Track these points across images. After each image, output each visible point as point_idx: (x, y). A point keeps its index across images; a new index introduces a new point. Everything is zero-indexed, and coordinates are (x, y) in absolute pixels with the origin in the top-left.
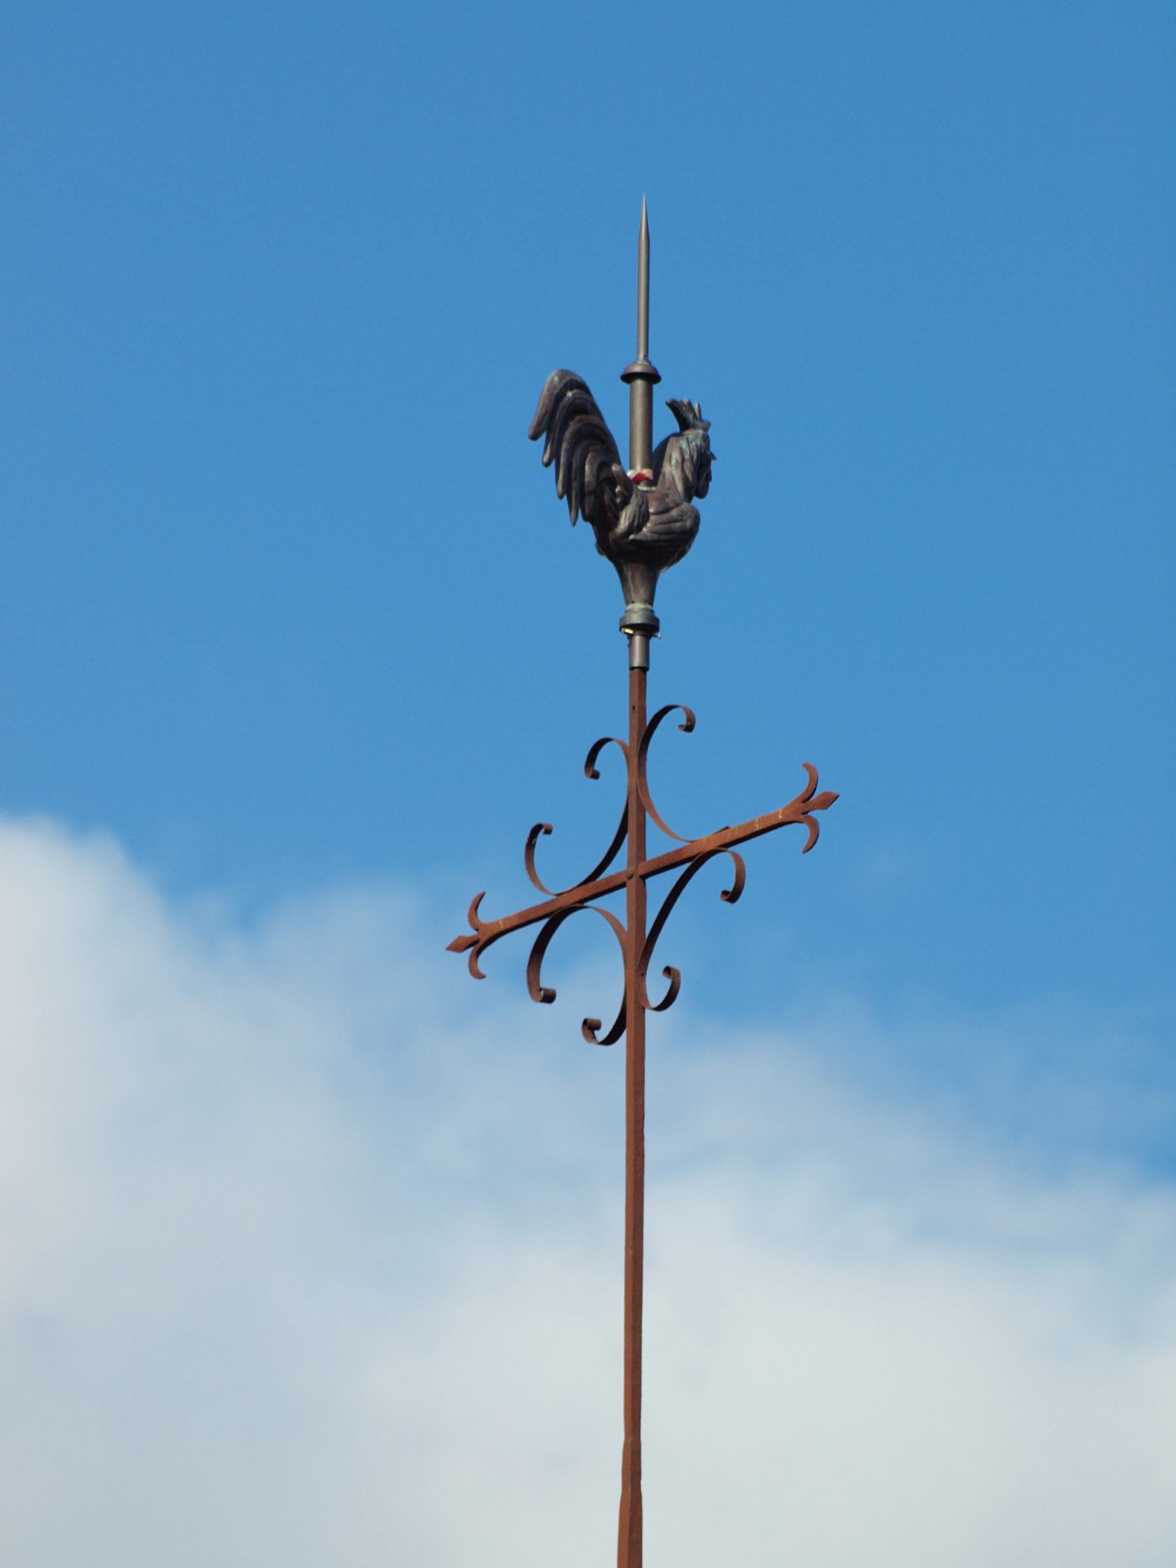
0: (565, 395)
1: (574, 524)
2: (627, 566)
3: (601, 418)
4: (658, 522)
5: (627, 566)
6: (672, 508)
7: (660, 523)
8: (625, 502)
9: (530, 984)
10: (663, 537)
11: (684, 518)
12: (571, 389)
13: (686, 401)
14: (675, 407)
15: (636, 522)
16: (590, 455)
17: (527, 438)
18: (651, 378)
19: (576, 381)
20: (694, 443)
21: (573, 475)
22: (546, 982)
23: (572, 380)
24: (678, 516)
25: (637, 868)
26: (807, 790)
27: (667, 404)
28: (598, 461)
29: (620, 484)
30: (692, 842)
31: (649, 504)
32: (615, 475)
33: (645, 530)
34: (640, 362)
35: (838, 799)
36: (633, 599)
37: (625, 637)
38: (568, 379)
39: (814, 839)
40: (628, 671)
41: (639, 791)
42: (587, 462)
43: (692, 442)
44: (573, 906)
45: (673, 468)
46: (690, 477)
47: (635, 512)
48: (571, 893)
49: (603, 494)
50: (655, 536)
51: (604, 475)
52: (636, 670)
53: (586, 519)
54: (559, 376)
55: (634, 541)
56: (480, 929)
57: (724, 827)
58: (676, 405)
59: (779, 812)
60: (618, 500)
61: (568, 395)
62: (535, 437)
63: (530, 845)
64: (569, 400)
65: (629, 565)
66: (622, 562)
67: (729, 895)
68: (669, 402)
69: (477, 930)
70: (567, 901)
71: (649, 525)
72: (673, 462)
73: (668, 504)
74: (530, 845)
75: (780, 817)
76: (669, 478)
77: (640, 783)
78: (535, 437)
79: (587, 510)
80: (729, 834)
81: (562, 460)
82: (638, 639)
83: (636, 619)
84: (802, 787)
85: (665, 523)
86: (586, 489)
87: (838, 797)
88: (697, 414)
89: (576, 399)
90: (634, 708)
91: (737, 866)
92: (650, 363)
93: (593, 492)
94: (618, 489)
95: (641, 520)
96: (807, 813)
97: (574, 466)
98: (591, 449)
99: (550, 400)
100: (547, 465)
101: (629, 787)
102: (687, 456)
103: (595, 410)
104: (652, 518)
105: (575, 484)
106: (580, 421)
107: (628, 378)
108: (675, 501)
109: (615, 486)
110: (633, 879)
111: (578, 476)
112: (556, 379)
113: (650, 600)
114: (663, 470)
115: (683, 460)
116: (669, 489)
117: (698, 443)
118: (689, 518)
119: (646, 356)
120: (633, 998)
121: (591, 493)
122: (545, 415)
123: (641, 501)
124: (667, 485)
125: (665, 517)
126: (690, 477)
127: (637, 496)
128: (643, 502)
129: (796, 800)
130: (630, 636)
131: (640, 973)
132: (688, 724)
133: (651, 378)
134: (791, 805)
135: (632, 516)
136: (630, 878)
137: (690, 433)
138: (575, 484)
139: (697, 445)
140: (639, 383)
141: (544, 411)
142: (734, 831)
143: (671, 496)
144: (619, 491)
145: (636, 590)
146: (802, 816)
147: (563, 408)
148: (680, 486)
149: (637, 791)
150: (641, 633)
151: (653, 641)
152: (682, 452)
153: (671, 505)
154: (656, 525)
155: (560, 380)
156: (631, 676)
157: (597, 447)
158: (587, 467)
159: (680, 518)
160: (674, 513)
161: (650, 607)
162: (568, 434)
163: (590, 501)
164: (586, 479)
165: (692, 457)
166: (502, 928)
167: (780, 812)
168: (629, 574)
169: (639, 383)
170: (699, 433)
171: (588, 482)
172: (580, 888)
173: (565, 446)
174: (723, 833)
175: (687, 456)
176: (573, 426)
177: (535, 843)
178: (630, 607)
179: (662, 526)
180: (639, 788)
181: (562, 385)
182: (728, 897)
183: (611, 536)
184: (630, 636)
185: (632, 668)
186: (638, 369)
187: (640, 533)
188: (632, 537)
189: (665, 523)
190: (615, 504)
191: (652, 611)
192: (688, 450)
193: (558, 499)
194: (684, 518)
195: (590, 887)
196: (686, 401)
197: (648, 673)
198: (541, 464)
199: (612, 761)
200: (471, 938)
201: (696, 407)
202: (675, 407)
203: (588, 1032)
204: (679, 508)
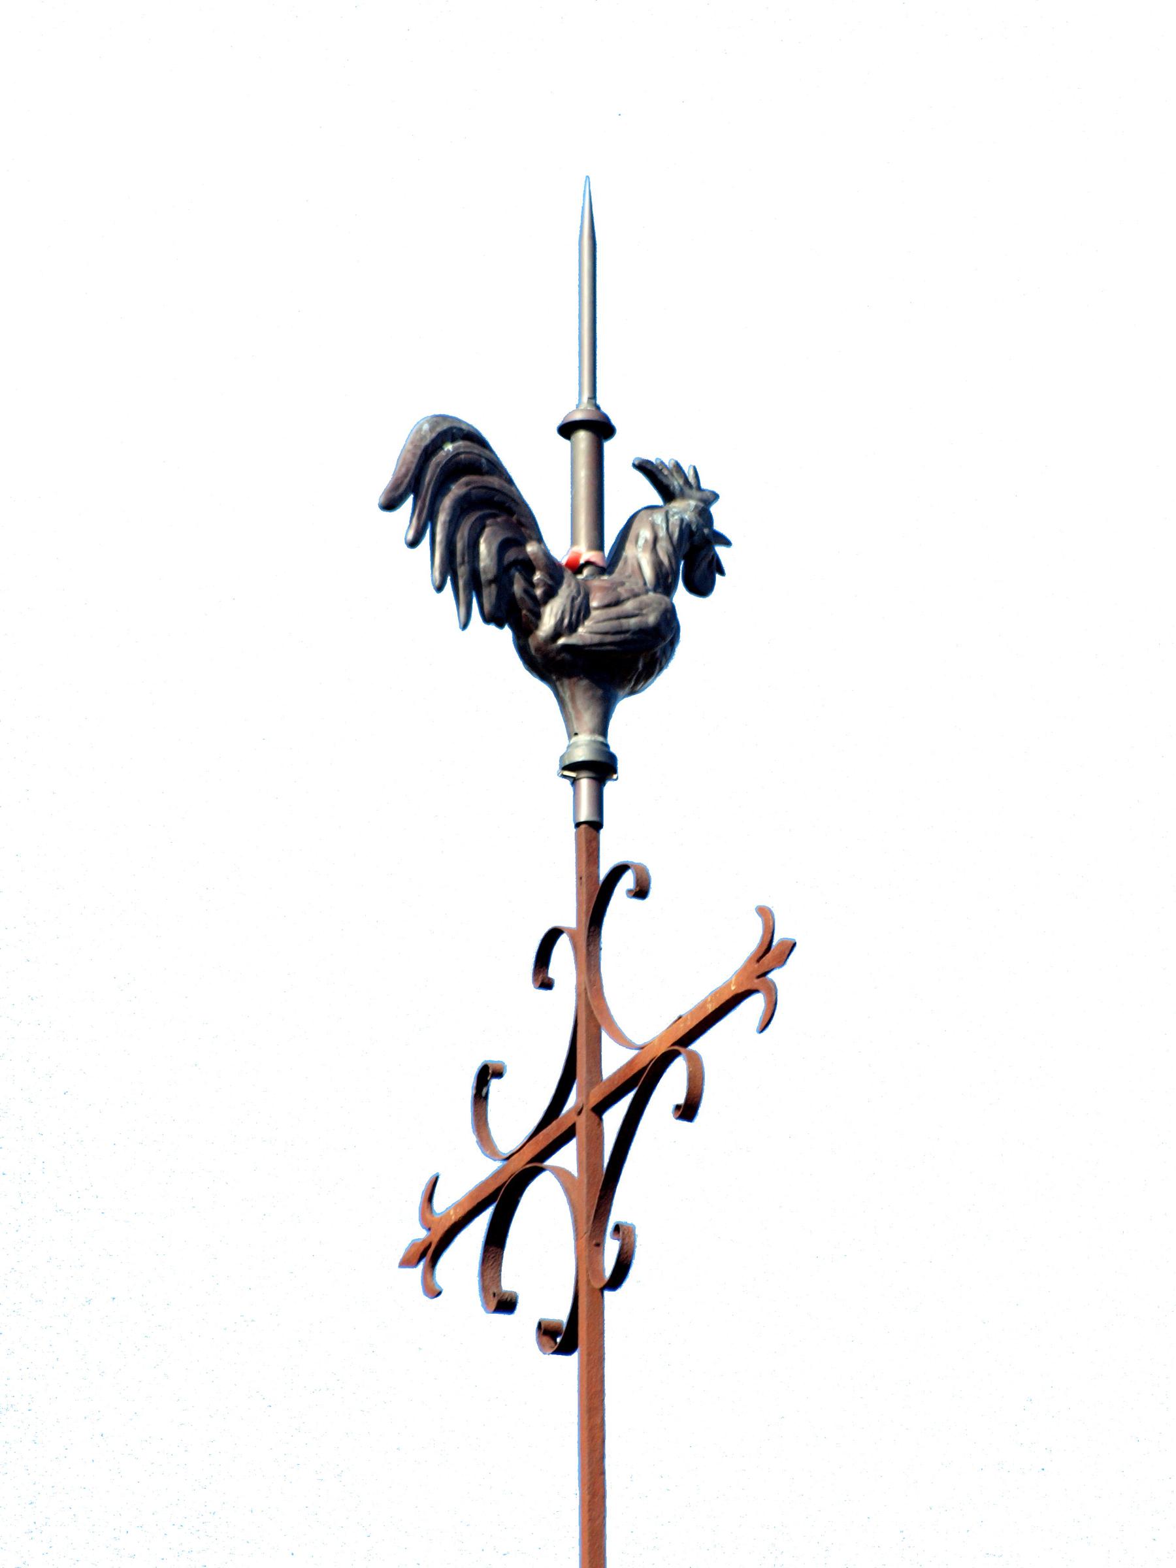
0: (441, 448)
1: (465, 626)
2: (562, 685)
3: (510, 481)
4: (601, 618)
5: (562, 685)
6: (628, 599)
7: (604, 620)
8: (550, 593)
9: (484, 1289)
10: (609, 638)
11: (644, 612)
12: (453, 440)
14: (646, 468)
15: (566, 621)
16: (487, 531)
18: (601, 429)
19: (461, 430)
20: (676, 517)
21: (459, 559)
22: (508, 1283)
24: (634, 609)
25: (588, 1097)
28: (500, 539)
29: (539, 570)
31: (591, 597)
32: (532, 558)
33: (581, 630)
35: (796, 950)
36: (577, 731)
37: (568, 782)
39: (772, 1008)
41: (589, 994)
42: (482, 541)
44: (524, 1168)
45: (640, 550)
47: (565, 606)
48: (522, 1151)
49: (511, 583)
50: (597, 639)
51: (511, 555)
53: (488, 619)
54: (430, 424)
55: (565, 647)
56: (432, 1226)
57: (676, 1018)
58: (649, 467)
59: (731, 982)
60: (539, 592)
61: (446, 449)
62: (390, 504)
63: (480, 1097)
64: (447, 454)
65: (566, 682)
66: (554, 677)
68: (636, 463)
70: (519, 1164)
71: (587, 623)
72: (641, 542)
73: (620, 594)
74: (480, 1097)
75: (733, 988)
76: (633, 565)
77: (590, 981)
78: (390, 504)
79: (487, 607)
80: (682, 1025)
82: (585, 784)
83: (581, 755)
84: (752, 941)
85: (610, 619)
86: (483, 578)
87: (794, 945)
88: (691, 479)
89: (458, 454)
90: (581, 878)
93: (494, 580)
94: (537, 576)
95: (574, 616)
96: (765, 974)
97: (460, 546)
98: (488, 522)
99: (414, 455)
100: (413, 544)
102: (662, 533)
103: (496, 467)
104: (594, 613)
105: (462, 571)
106: (467, 484)
108: (632, 590)
109: (533, 573)
111: (466, 558)
112: (426, 427)
113: (603, 729)
115: (656, 539)
116: (630, 576)
117: (686, 517)
118: (654, 610)
120: (585, 1279)
121: (490, 582)
122: (405, 475)
123: (575, 591)
124: (629, 571)
125: (614, 611)
127: (569, 586)
128: (579, 593)
129: (750, 960)
130: (574, 781)
131: (594, 1242)
132: (638, 889)
133: (601, 429)
135: (560, 612)
139: (682, 520)
140: (582, 436)
141: (403, 470)
142: (686, 1019)
143: (627, 584)
144: (538, 579)
145: (578, 719)
146: (756, 981)
147: (438, 464)
148: (648, 573)
149: (586, 993)
150: (591, 774)
151: (609, 788)
152: (654, 527)
153: (625, 595)
154: (598, 622)
155: (432, 429)
157: (499, 520)
158: (483, 548)
159: (637, 612)
160: (629, 606)
161: (601, 739)
162: (447, 503)
163: (490, 593)
164: (482, 564)
165: (670, 535)
166: (454, 1218)
167: (733, 982)
168: (567, 696)
169: (583, 437)
170: (689, 505)
171: (485, 567)
174: (675, 1025)
175: (662, 533)
176: (456, 490)
178: (574, 739)
180: (588, 990)
181: (434, 435)
182: (680, 1113)
183: (532, 642)
186: (579, 416)
187: (574, 635)
188: (562, 641)
189: (610, 619)
190: (533, 597)
191: (607, 746)
192: (664, 525)
194: (644, 612)
195: (541, 1137)
197: (602, 831)
199: (563, 956)
200: (424, 1241)
201: (686, 468)
202: (646, 468)
203: (545, 1339)
204: (638, 600)
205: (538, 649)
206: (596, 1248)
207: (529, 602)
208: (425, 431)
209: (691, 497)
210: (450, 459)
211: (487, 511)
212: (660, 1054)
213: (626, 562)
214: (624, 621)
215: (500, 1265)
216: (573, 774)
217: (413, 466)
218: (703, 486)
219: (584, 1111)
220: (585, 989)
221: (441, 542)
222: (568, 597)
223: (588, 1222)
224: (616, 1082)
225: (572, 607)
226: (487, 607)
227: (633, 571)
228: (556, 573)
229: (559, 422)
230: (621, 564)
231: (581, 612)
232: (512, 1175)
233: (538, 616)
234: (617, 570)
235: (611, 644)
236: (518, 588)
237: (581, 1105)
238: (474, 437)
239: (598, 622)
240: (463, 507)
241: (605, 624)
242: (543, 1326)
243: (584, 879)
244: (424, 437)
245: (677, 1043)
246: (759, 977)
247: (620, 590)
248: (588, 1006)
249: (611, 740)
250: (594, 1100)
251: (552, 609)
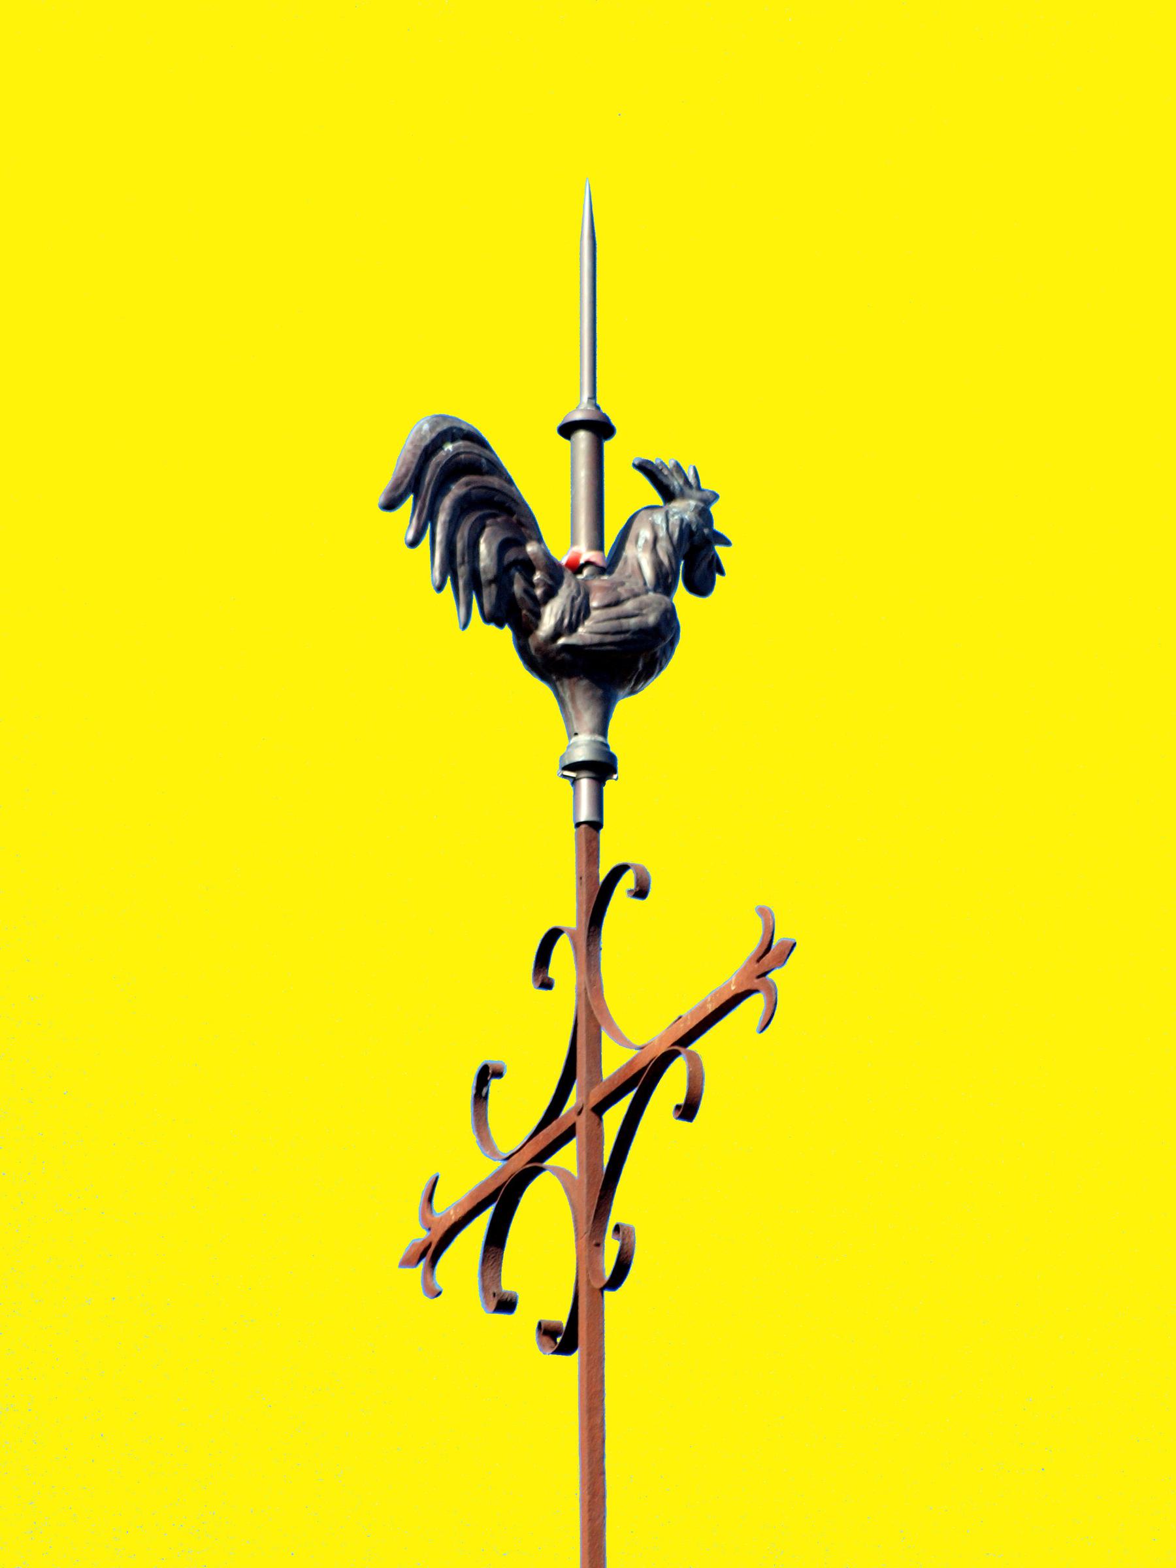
0: (441, 448)
1: (465, 626)
2: (562, 685)
3: (510, 481)
4: (601, 618)
5: (562, 685)
6: (628, 599)
7: (604, 620)
8: (550, 593)
9: (484, 1289)
10: (609, 638)
11: (644, 612)
12: (453, 440)
14: (646, 469)
15: (566, 621)
16: (487, 531)
17: (377, 506)
18: (601, 429)
19: (461, 430)
20: (676, 517)
21: (459, 559)
22: (508, 1283)
23: (451, 429)
24: (634, 609)
26: (760, 946)
28: (500, 539)
29: (539, 570)
30: (642, 1048)
31: (591, 597)
32: (532, 558)
33: (581, 630)
36: (577, 731)
37: (568, 782)
39: (772, 1008)
40: (574, 830)
42: (482, 541)
43: (673, 516)
44: (524, 1168)
45: (640, 550)
46: (666, 561)
47: (565, 606)
48: (522, 1151)
49: (511, 583)
50: (597, 639)
51: (511, 555)
53: (488, 619)
54: (430, 424)
55: (565, 647)
57: (676, 1018)
58: (649, 467)
59: (731, 982)
60: (539, 592)
61: (446, 449)
62: (391, 504)
63: (480, 1097)
64: (447, 454)
65: (566, 682)
66: (554, 677)
68: (636, 463)
70: (519, 1164)
71: (587, 623)
72: (641, 542)
73: (620, 594)
74: (480, 1097)
76: (633, 565)
77: (590, 981)
78: (391, 504)
79: (487, 607)
80: (682, 1025)
81: (439, 537)
82: (585, 784)
84: (752, 941)
85: (610, 619)
86: (483, 578)
87: (795, 944)
88: (691, 479)
89: (458, 454)
90: (581, 878)
91: (689, 1067)
93: (494, 580)
94: (537, 576)
95: (574, 616)
97: (460, 546)
98: (488, 522)
99: (414, 455)
100: (414, 544)
102: (662, 533)
103: (495, 467)
104: (594, 613)
105: (462, 571)
106: (467, 484)
107: (567, 430)
108: (632, 590)
109: (533, 573)
110: (582, 1114)
111: (466, 558)
112: (426, 427)
113: (603, 729)
115: (656, 539)
116: (630, 576)
117: (686, 517)
118: (654, 610)
119: (593, 396)
121: (490, 582)
122: (405, 475)
123: (575, 591)
124: (629, 571)
125: (614, 611)
127: (569, 586)
128: (579, 593)
130: (574, 781)
131: (594, 1242)
132: (638, 889)
133: (601, 429)
135: (560, 612)
136: (580, 1113)
138: (462, 571)
139: (682, 520)
140: (582, 436)
141: (403, 470)
142: (686, 1020)
143: (627, 584)
144: (538, 579)
145: (578, 719)
146: (756, 981)
147: (438, 464)
148: (648, 573)
149: (586, 993)
150: (591, 774)
152: (654, 527)
153: (625, 595)
154: (598, 622)
155: (432, 429)
156: (577, 836)
157: (499, 520)
158: (483, 548)
159: (637, 612)
160: (629, 606)
161: (601, 739)
162: (447, 503)
163: (490, 593)
164: (482, 564)
166: (454, 1218)
167: (733, 982)
168: (567, 696)
169: (583, 437)
170: (689, 505)
171: (485, 567)
173: (442, 518)
174: (675, 1025)
175: (662, 533)
176: (456, 490)
178: (574, 739)
179: (615, 623)
180: (588, 990)
181: (434, 435)
183: (532, 642)
184: (574, 781)
186: (579, 416)
187: (574, 635)
188: (562, 641)
189: (610, 619)
190: (533, 597)
191: (607, 746)
192: (664, 525)
193: (434, 591)
194: (644, 612)
195: (541, 1137)
196: (670, 464)
197: (602, 831)
198: (404, 542)
199: (563, 955)
200: (424, 1241)
202: (646, 469)
204: (638, 600)
206: (596, 1248)
207: (529, 602)
208: (425, 431)
209: (691, 497)
210: (450, 459)
211: (487, 511)
212: (660, 1054)
213: (626, 562)
214: (624, 621)
215: (500, 1265)
216: (573, 774)
217: (413, 466)
218: (703, 486)
219: (584, 1111)
220: (585, 989)
221: (441, 542)
222: (568, 597)
223: (588, 1222)
224: (616, 1082)
225: (572, 607)
226: (487, 607)
227: (633, 571)
228: (555, 574)
230: (621, 564)
231: (581, 612)
232: (512, 1175)
233: (538, 616)
234: (617, 570)
235: (611, 644)
236: (518, 588)
237: (581, 1105)
239: (598, 622)
240: (463, 507)
241: (605, 624)
242: (543, 1326)
244: (424, 437)
245: (677, 1043)
247: (620, 590)
249: (611, 740)
250: (594, 1100)
251: (552, 609)
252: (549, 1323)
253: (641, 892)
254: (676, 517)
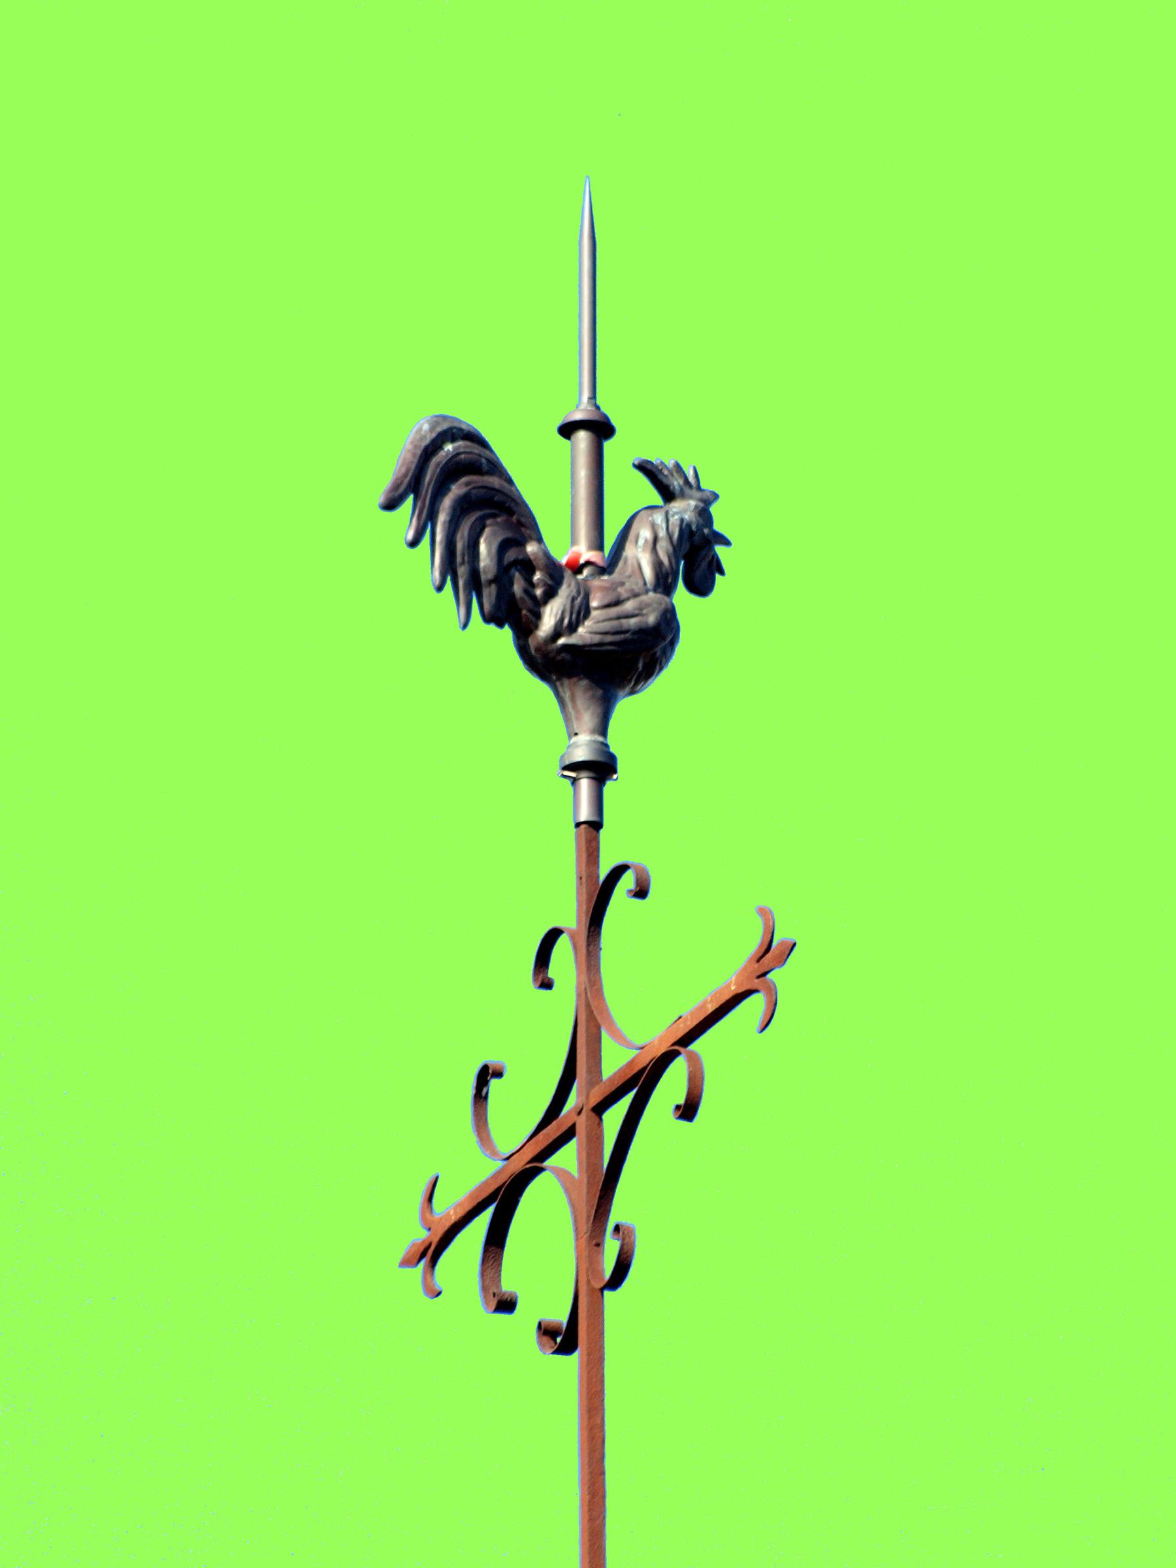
0: (441, 448)
1: (465, 626)
2: (562, 685)
3: (510, 481)
4: (601, 618)
5: (562, 685)
6: (628, 599)
7: (604, 620)
8: (550, 593)
9: (484, 1289)
10: (609, 638)
11: (644, 612)
12: (453, 440)
13: (670, 463)
14: (646, 469)
15: (566, 621)
16: (487, 531)
18: (601, 429)
19: (461, 430)
20: (676, 517)
21: (459, 559)
22: (508, 1283)
23: (451, 429)
24: (634, 609)
26: (761, 945)
27: (634, 465)
28: (500, 539)
29: (539, 570)
30: (642, 1048)
31: (591, 597)
32: (532, 558)
33: (581, 630)
34: (582, 407)
36: (577, 731)
37: (568, 782)
38: (445, 426)
39: (772, 1008)
40: (573, 830)
41: (589, 994)
42: (482, 541)
43: (673, 516)
44: (524, 1168)
45: (640, 550)
46: (666, 561)
48: (521, 1151)
49: (511, 583)
50: (597, 639)
51: (511, 555)
52: (583, 826)
53: (488, 619)
54: (430, 424)
55: (565, 647)
57: (676, 1018)
58: (649, 467)
59: (731, 982)
60: (539, 592)
61: (446, 449)
62: (391, 505)
63: (480, 1097)
64: (447, 454)
66: (554, 677)
67: (681, 1110)
68: (636, 463)
69: (429, 1229)
70: (519, 1164)
71: (587, 623)
72: (641, 542)
73: (620, 594)
74: (480, 1097)
76: (633, 565)
78: (391, 505)
79: (487, 607)
81: (439, 537)
82: (585, 784)
84: (752, 942)
85: (610, 619)
86: (483, 578)
87: (794, 945)
88: (691, 479)
89: (458, 454)
90: (581, 878)
91: (689, 1067)
92: (598, 408)
93: (494, 580)
94: (537, 576)
95: (574, 616)
96: (764, 974)
97: (460, 546)
98: (488, 522)
99: (414, 455)
100: (414, 544)
101: (578, 988)
102: (662, 533)
103: (495, 468)
104: (594, 613)
106: (467, 484)
107: (567, 430)
108: (632, 590)
109: (533, 573)
112: (426, 427)
113: (603, 729)
114: (624, 554)
115: (656, 539)
116: (630, 576)
117: (686, 517)
118: (654, 610)
119: (593, 396)
120: (585, 1279)
121: (490, 582)
122: (405, 475)
123: (575, 591)
124: (629, 571)
125: (614, 611)
126: (666, 561)
127: (569, 586)
128: (579, 593)
130: (574, 781)
131: (594, 1242)
132: (638, 889)
133: (601, 429)
134: (745, 969)
135: (560, 612)
136: (580, 1113)
137: (676, 506)
140: (582, 436)
141: (403, 470)
142: (686, 1020)
143: (627, 584)
144: (538, 579)
145: (578, 719)
146: (756, 981)
147: (438, 464)
148: (648, 573)
149: (586, 993)
150: (591, 774)
151: (609, 787)
152: (654, 527)
153: (625, 595)
154: (598, 622)
155: (432, 429)
156: (578, 836)
157: (499, 520)
158: (483, 548)
159: (637, 612)
160: (629, 606)
161: (601, 739)
162: (447, 503)
163: (490, 593)
164: (482, 564)
165: (670, 535)
166: (454, 1218)
167: (733, 983)
168: (567, 696)
169: (583, 437)
170: (689, 505)
171: (485, 567)
172: (531, 1142)
175: (662, 533)
176: (456, 490)
177: (487, 1093)
178: (574, 739)
179: (615, 623)
180: (588, 990)
181: (434, 435)
182: (680, 1113)
183: (532, 642)
184: (574, 781)
185: (578, 825)
186: (579, 416)
187: (574, 635)
188: (562, 641)
189: (610, 619)
190: (533, 597)
191: (607, 746)
192: (664, 525)
193: (434, 591)
194: (644, 612)
195: (541, 1137)
197: (602, 831)
199: (563, 955)
200: (424, 1241)
202: (646, 469)
203: (545, 1339)
204: (638, 600)
205: (538, 649)
206: (596, 1248)
207: (529, 602)
208: (425, 431)
209: (691, 497)
210: (450, 459)
211: (487, 511)
212: (660, 1054)
213: (626, 562)
214: (624, 621)
215: (500, 1265)
216: (573, 774)
217: (413, 466)
218: (703, 486)
219: (584, 1111)
220: (586, 989)
221: (441, 542)
222: (568, 597)
223: (588, 1222)
224: (616, 1082)
225: (572, 607)
226: (487, 607)
229: (559, 422)
230: (621, 564)
231: (581, 612)
232: (512, 1175)
233: (538, 616)
234: (617, 570)
235: (611, 644)
236: (518, 588)
237: (581, 1105)
238: (473, 437)
239: (598, 622)
240: (463, 507)
241: (605, 624)
243: (584, 879)
244: (424, 437)
245: (677, 1043)
246: (759, 977)
247: (620, 590)
248: (588, 1006)
249: (611, 740)
251: (552, 609)
252: (549, 1323)
253: (641, 892)
254: (676, 517)
